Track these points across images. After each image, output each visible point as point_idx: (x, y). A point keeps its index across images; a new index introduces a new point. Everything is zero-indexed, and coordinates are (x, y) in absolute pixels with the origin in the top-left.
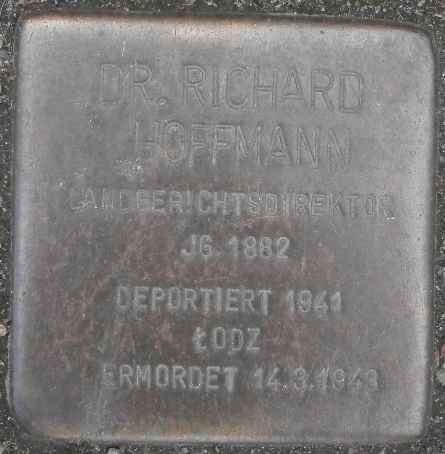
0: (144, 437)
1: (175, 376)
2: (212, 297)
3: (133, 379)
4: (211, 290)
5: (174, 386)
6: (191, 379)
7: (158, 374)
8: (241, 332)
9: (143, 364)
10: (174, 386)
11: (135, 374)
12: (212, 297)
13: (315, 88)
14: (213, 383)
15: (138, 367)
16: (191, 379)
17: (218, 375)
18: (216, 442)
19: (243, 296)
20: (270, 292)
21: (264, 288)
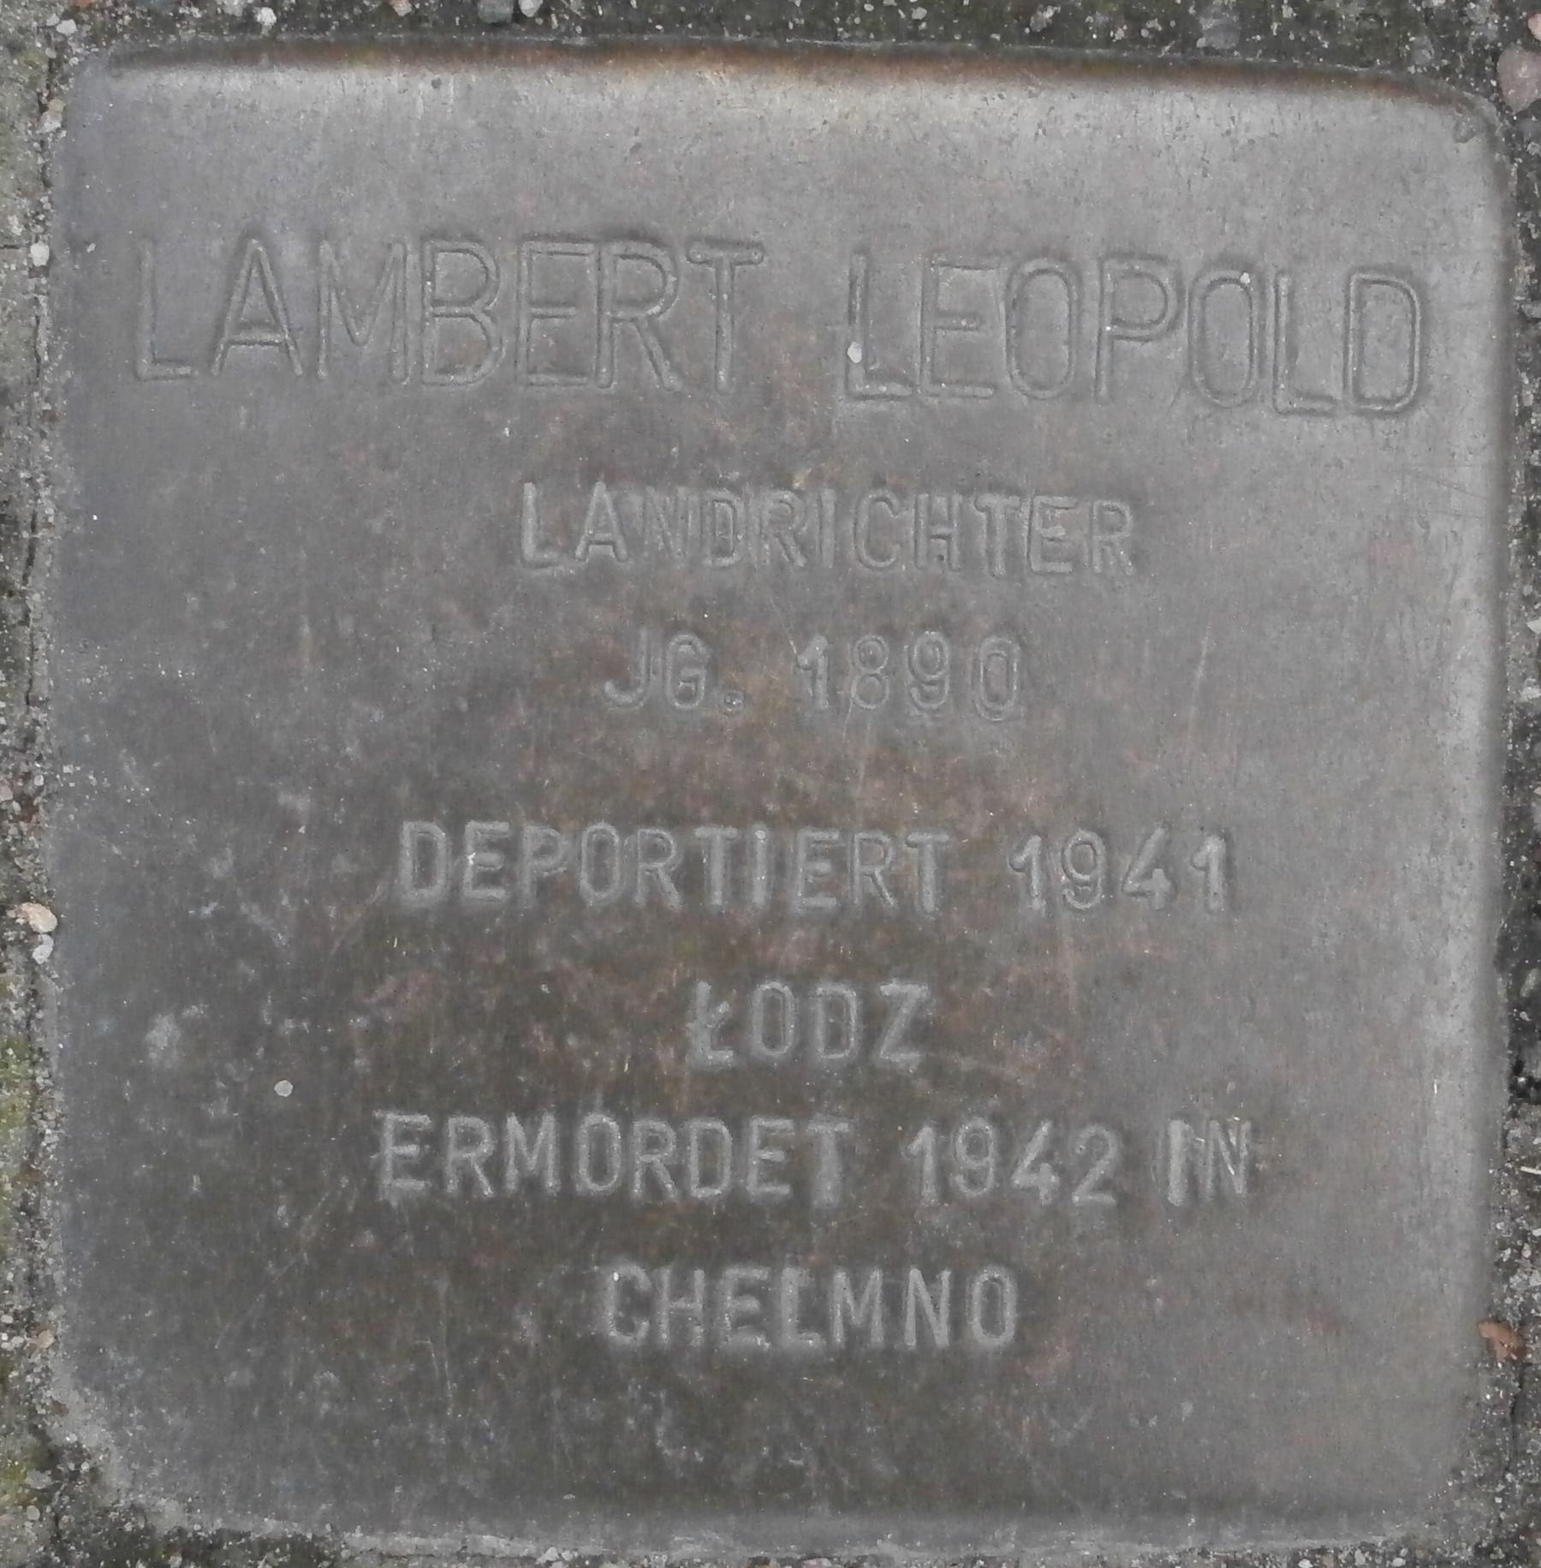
0: (745, 1339)
1: (641, 1159)
2: (738, 854)
3: (495, 1167)
4: (731, 832)
5: (637, 1189)
6: (694, 1171)
7: (584, 1148)
8: (851, 995)
9: (528, 1112)
10: (637, 1189)
11: (500, 1147)
12: (738, 854)
13: (932, 522)
14: (772, 1172)
15: (512, 1122)
16: (694, 1171)
17: (788, 1151)
18: (328, 72)
19: (862, 766)
20: (844, 1127)
21: (1003, 491)
